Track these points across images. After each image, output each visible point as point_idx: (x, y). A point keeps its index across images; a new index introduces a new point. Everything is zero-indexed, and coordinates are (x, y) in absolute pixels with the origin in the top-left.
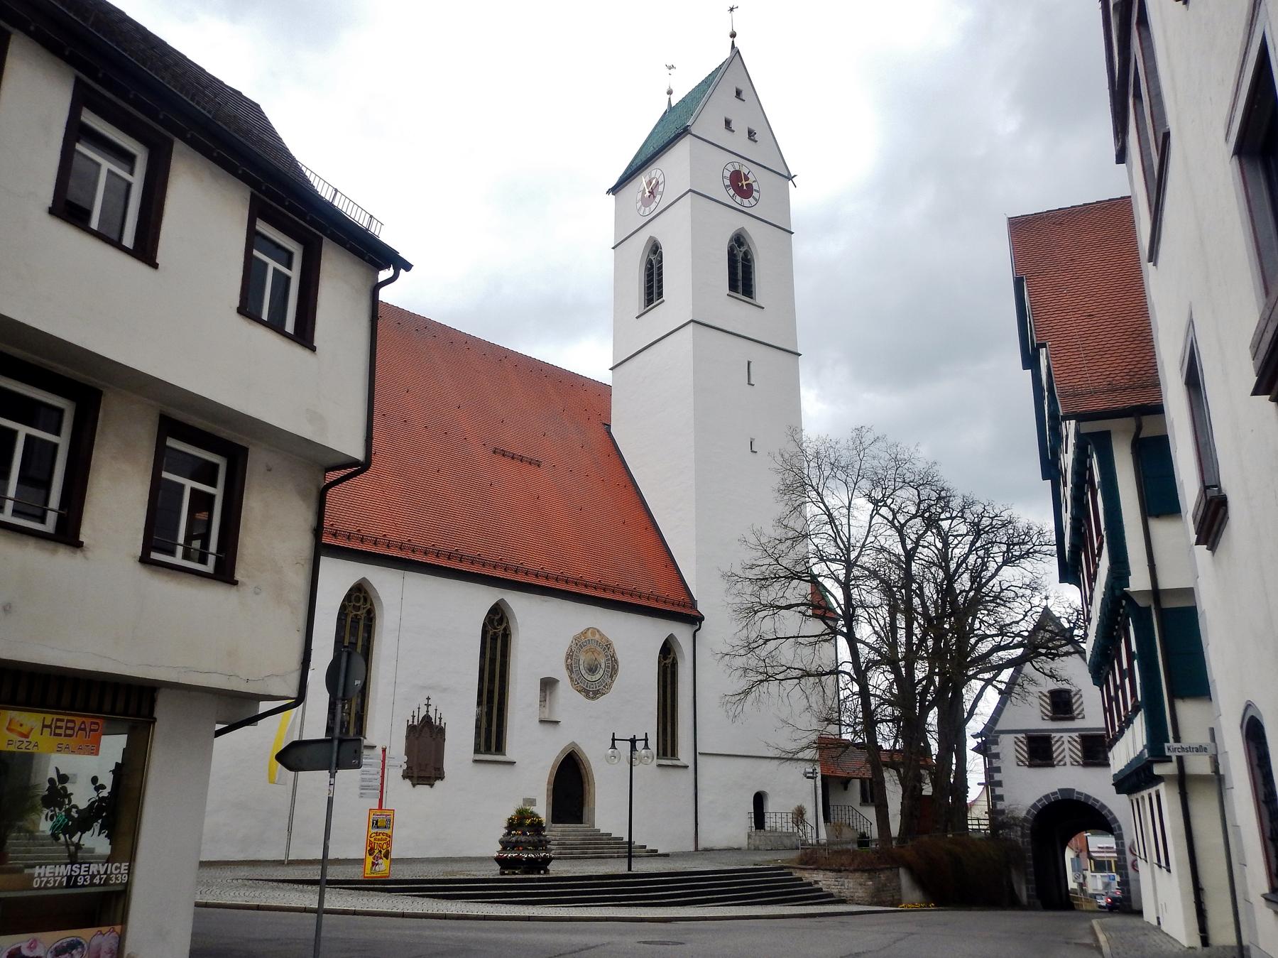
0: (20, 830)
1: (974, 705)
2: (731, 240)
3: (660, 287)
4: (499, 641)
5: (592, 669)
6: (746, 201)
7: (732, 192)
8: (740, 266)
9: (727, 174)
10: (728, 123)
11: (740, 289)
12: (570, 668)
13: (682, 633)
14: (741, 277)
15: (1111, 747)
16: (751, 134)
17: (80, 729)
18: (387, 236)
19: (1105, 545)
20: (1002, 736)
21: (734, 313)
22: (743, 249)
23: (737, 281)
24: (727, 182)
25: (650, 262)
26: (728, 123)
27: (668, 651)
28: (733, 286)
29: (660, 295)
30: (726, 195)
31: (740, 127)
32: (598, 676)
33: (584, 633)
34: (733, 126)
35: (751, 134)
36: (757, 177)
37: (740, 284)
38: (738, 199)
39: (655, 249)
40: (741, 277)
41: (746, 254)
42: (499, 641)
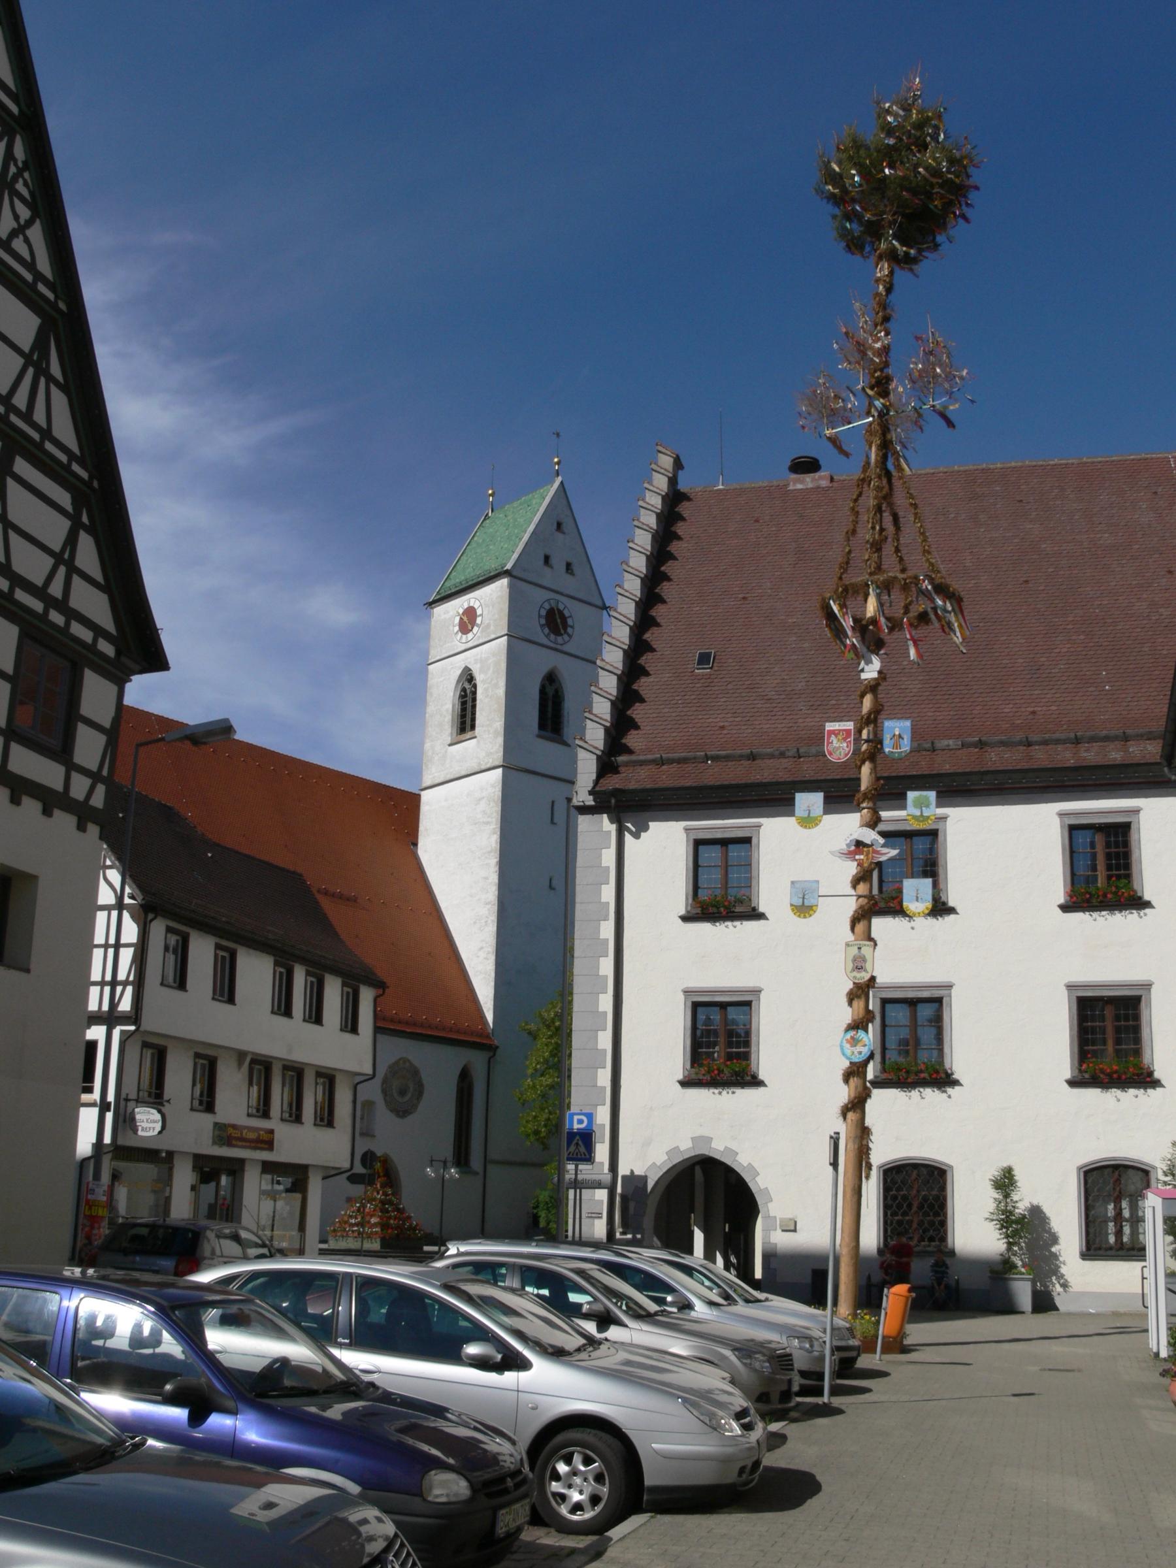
2: (543, 679)
3: (473, 719)
4: (550, 715)
5: (402, 1093)
7: (547, 630)
8: (550, 704)
9: (543, 613)
10: (547, 559)
12: (384, 1092)
13: (477, 1060)
16: (569, 567)
18: (705, 927)
19: (107, 761)
26: (547, 559)
27: (465, 1077)
28: (542, 726)
29: (473, 727)
30: (541, 636)
31: (558, 563)
32: (407, 1098)
33: (397, 1063)
34: (553, 561)
35: (569, 567)
36: (578, 614)
38: (552, 637)
41: (557, 691)
42: (550, 715)
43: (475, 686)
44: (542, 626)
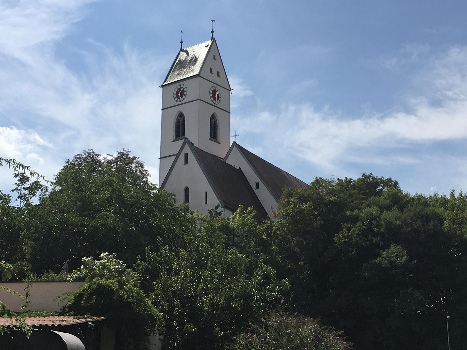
9: (211, 92)
10: (211, 69)
26: (211, 69)
28: (211, 136)
36: (220, 91)
39: (181, 115)
43: (184, 119)
44: (211, 97)
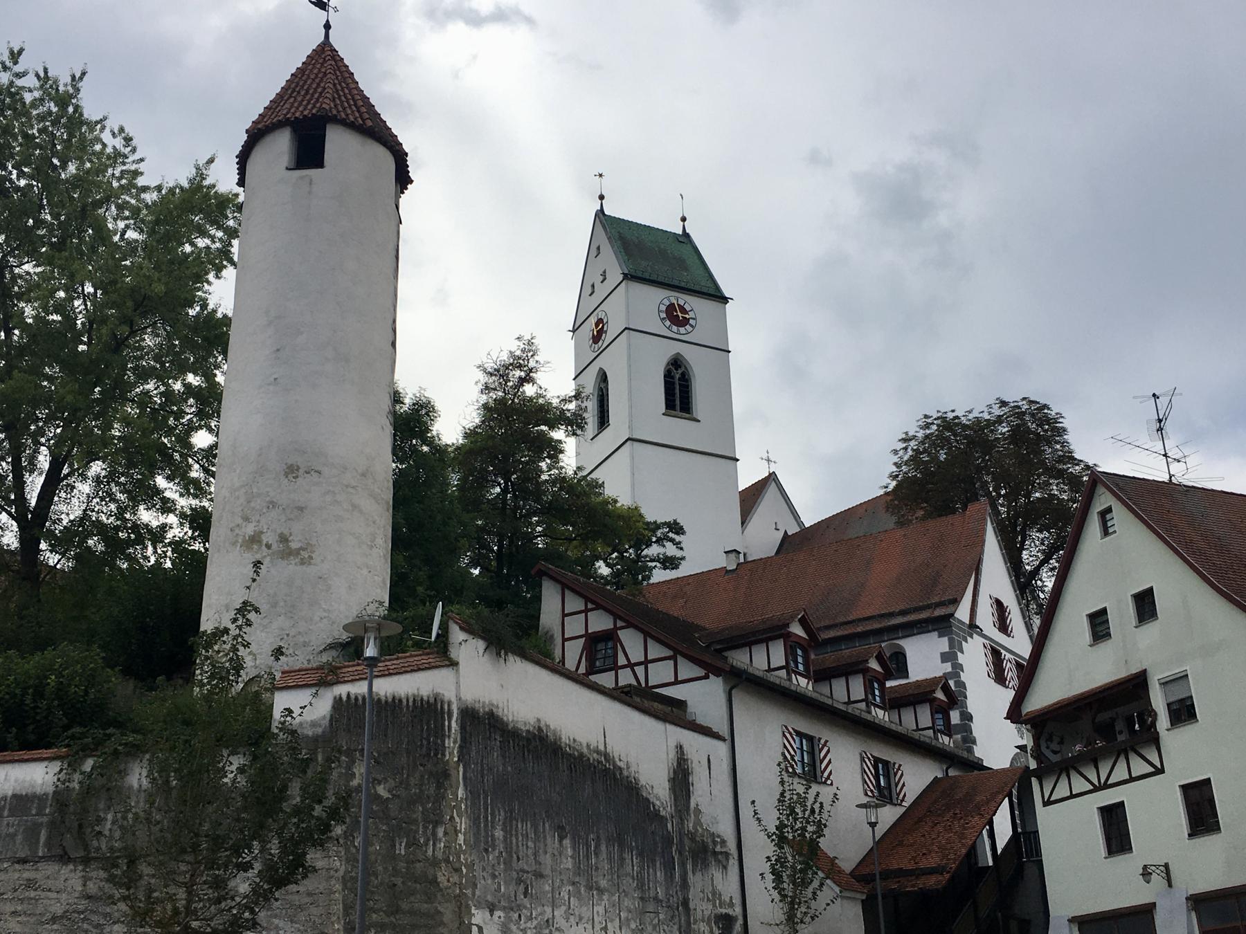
0: (535, 827)
1: (579, 662)
6: (682, 330)
7: (668, 323)
9: (663, 308)
11: (678, 407)
14: (678, 393)
15: (524, 656)
17: (240, 628)
20: (374, 689)
21: (676, 429)
22: (680, 371)
23: (674, 395)
24: (664, 315)
25: (601, 389)
28: (670, 405)
37: (678, 402)
38: (675, 328)
39: (603, 377)
40: (678, 393)
41: (683, 374)
